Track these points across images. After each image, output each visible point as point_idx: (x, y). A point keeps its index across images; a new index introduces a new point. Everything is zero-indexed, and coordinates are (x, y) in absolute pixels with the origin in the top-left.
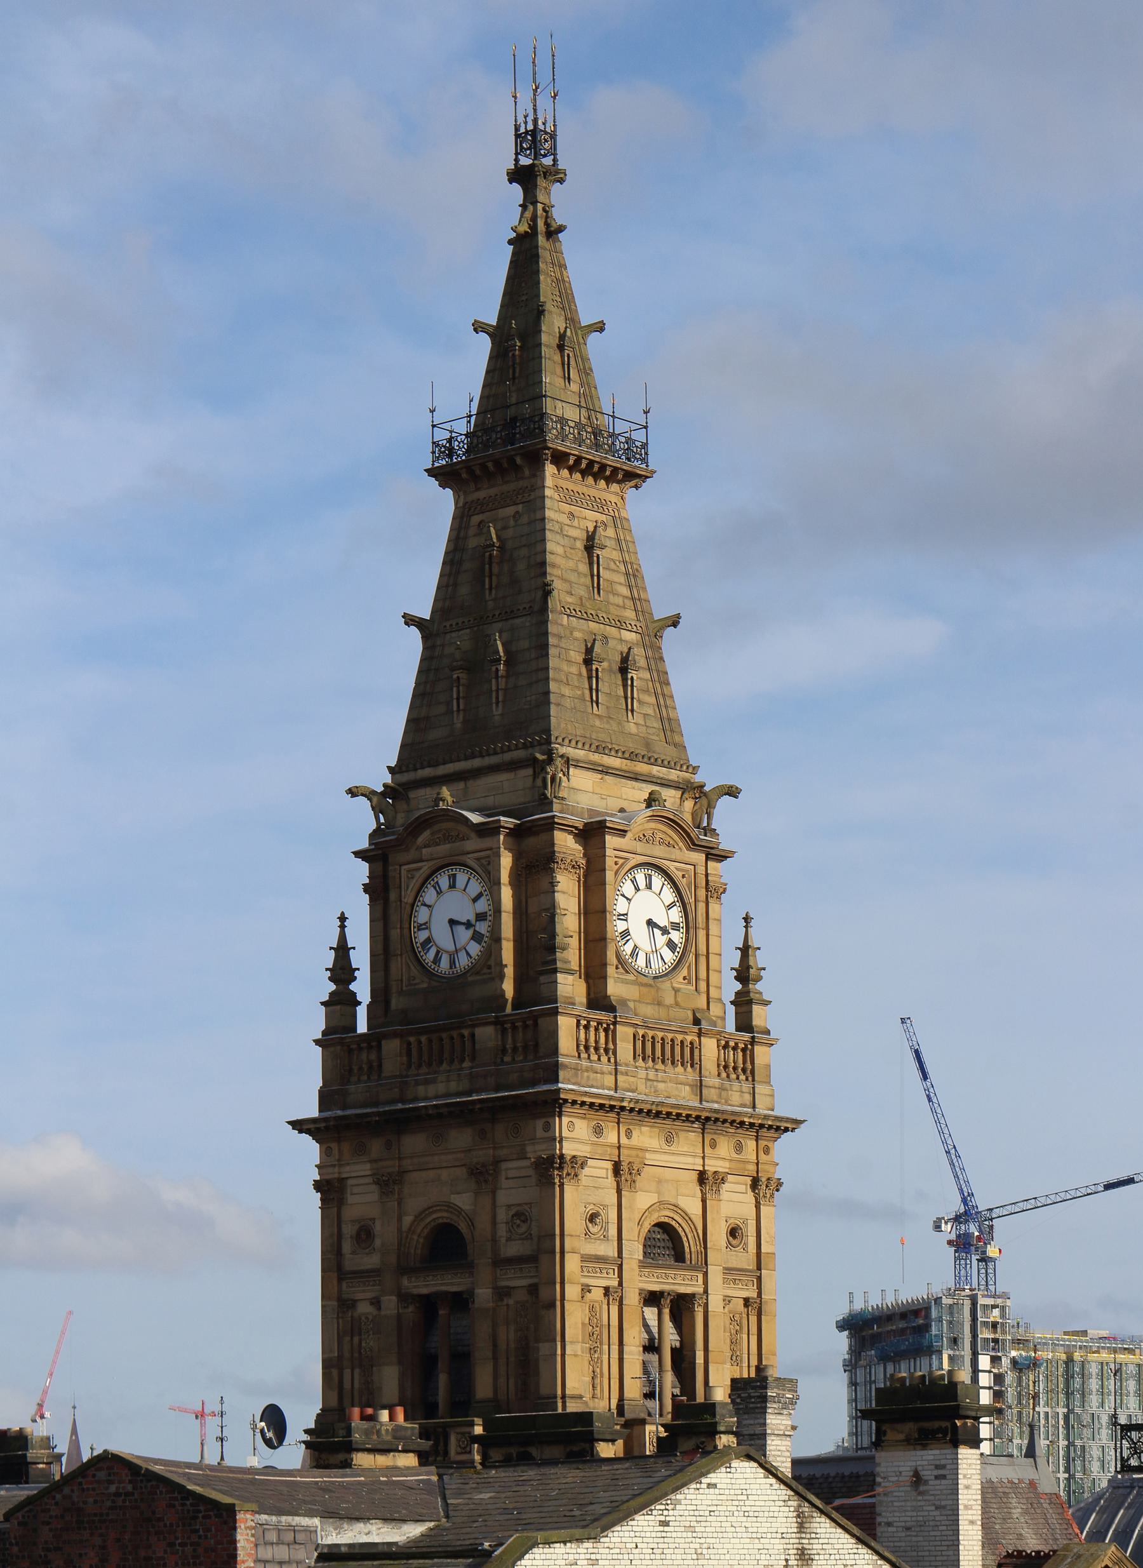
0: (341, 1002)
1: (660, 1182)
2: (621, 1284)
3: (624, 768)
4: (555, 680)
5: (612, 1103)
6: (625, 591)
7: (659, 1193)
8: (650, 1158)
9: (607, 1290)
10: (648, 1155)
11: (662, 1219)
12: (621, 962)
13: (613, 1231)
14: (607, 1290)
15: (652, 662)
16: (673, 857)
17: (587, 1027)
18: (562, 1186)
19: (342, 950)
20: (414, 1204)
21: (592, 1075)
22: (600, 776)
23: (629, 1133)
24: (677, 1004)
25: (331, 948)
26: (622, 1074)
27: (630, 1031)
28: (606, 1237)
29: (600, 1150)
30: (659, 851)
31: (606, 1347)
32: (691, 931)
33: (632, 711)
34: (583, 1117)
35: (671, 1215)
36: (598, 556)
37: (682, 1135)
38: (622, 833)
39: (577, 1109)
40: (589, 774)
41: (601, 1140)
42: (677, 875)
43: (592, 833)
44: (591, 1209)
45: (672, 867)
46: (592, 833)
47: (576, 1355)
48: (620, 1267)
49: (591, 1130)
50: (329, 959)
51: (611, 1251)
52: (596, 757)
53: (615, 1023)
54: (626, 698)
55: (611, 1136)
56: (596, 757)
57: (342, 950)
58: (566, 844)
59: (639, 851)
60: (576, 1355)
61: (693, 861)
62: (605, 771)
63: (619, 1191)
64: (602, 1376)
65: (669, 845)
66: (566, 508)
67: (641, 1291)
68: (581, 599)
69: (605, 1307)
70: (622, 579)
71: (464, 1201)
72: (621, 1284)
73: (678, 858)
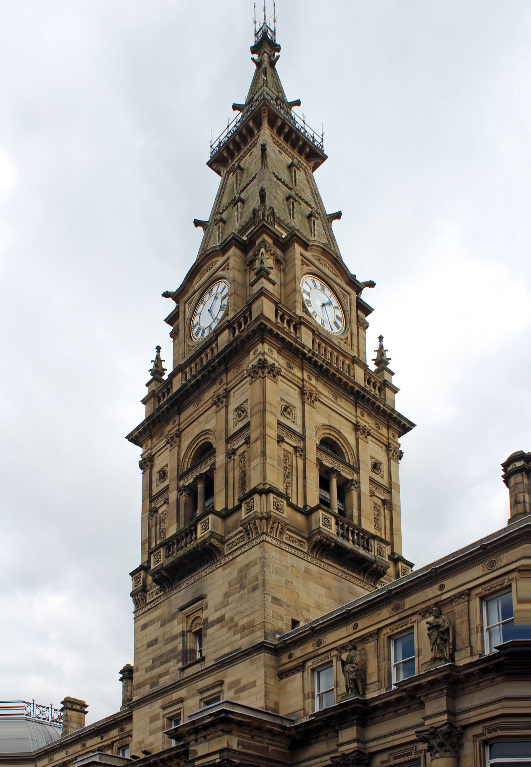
0: (157, 370)
7: (329, 420)
19: (158, 361)
20: (186, 441)
32: (348, 324)
50: (151, 366)
57: (158, 361)
71: (351, 438)
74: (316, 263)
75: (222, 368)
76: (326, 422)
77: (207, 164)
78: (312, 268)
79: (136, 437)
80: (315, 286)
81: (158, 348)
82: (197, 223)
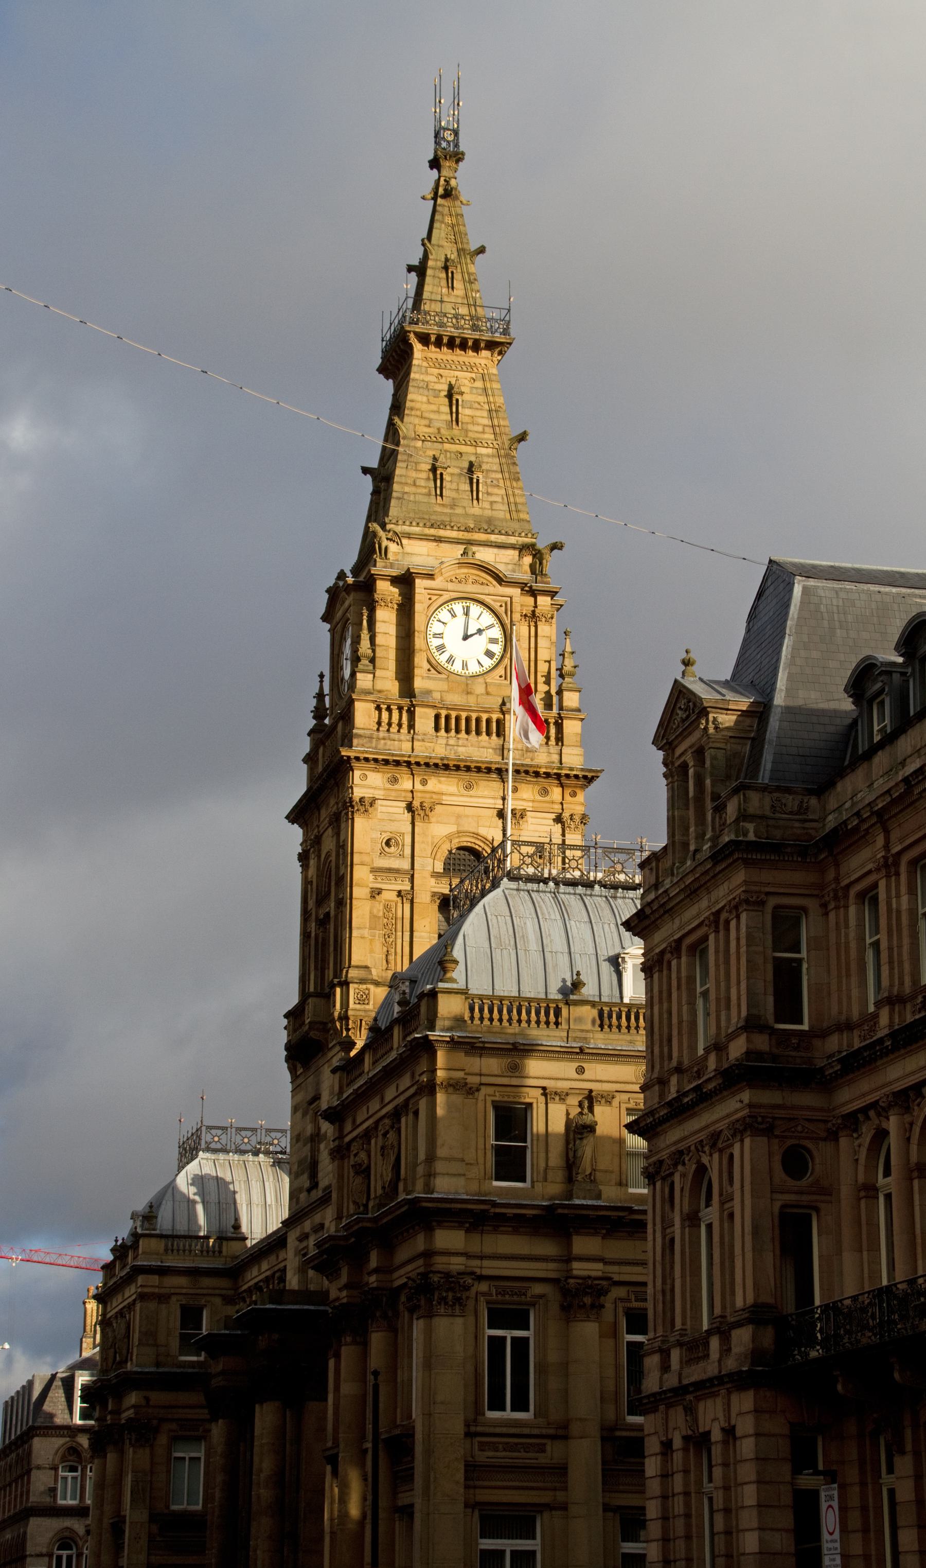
1: (459, 817)
2: (412, 888)
3: (460, 537)
4: (398, 483)
5: (367, 756)
6: (487, 422)
7: (458, 825)
8: (446, 799)
9: (399, 893)
10: (444, 797)
11: (465, 844)
12: (434, 666)
13: (408, 851)
14: (399, 893)
15: (505, 466)
16: (487, 592)
17: (389, 709)
18: (353, 819)
21: (389, 742)
22: (435, 544)
23: (424, 782)
24: (488, 693)
25: (365, 470)
26: (418, 740)
27: (432, 713)
28: (402, 856)
29: (393, 794)
30: (470, 588)
31: (399, 934)
33: (478, 499)
34: (375, 770)
35: (473, 840)
36: (457, 400)
37: (483, 784)
38: (431, 576)
39: (363, 764)
40: (424, 543)
41: (396, 787)
42: (496, 606)
43: (405, 581)
44: (386, 836)
45: (488, 600)
46: (405, 581)
47: (362, 938)
48: (413, 876)
49: (385, 780)
51: (406, 865)
52: (432, 531)
53: (414, 706)
54: (472, 491)
55: (406, 783)
56: (432, 531)
58: (384, 588)
59: (449, 588)
60: (362, 938)
61: (511, 594)
62: (439, 540)
63: (413, 824)
64: (396, 954)
65: (482, 584)
66: (436, 371)
67: (434, 894)
68: (439, 429)
69: (400, 905)
70: (485, 414)
72: (412, 888)
73: (492, 592)
74: (450, 586)
75: (333, 782)
76: (453, 829)
78: (447, 596)
79: (298, 815)
80: (454, 616)
81: (322, 676)
82: (365, 470)
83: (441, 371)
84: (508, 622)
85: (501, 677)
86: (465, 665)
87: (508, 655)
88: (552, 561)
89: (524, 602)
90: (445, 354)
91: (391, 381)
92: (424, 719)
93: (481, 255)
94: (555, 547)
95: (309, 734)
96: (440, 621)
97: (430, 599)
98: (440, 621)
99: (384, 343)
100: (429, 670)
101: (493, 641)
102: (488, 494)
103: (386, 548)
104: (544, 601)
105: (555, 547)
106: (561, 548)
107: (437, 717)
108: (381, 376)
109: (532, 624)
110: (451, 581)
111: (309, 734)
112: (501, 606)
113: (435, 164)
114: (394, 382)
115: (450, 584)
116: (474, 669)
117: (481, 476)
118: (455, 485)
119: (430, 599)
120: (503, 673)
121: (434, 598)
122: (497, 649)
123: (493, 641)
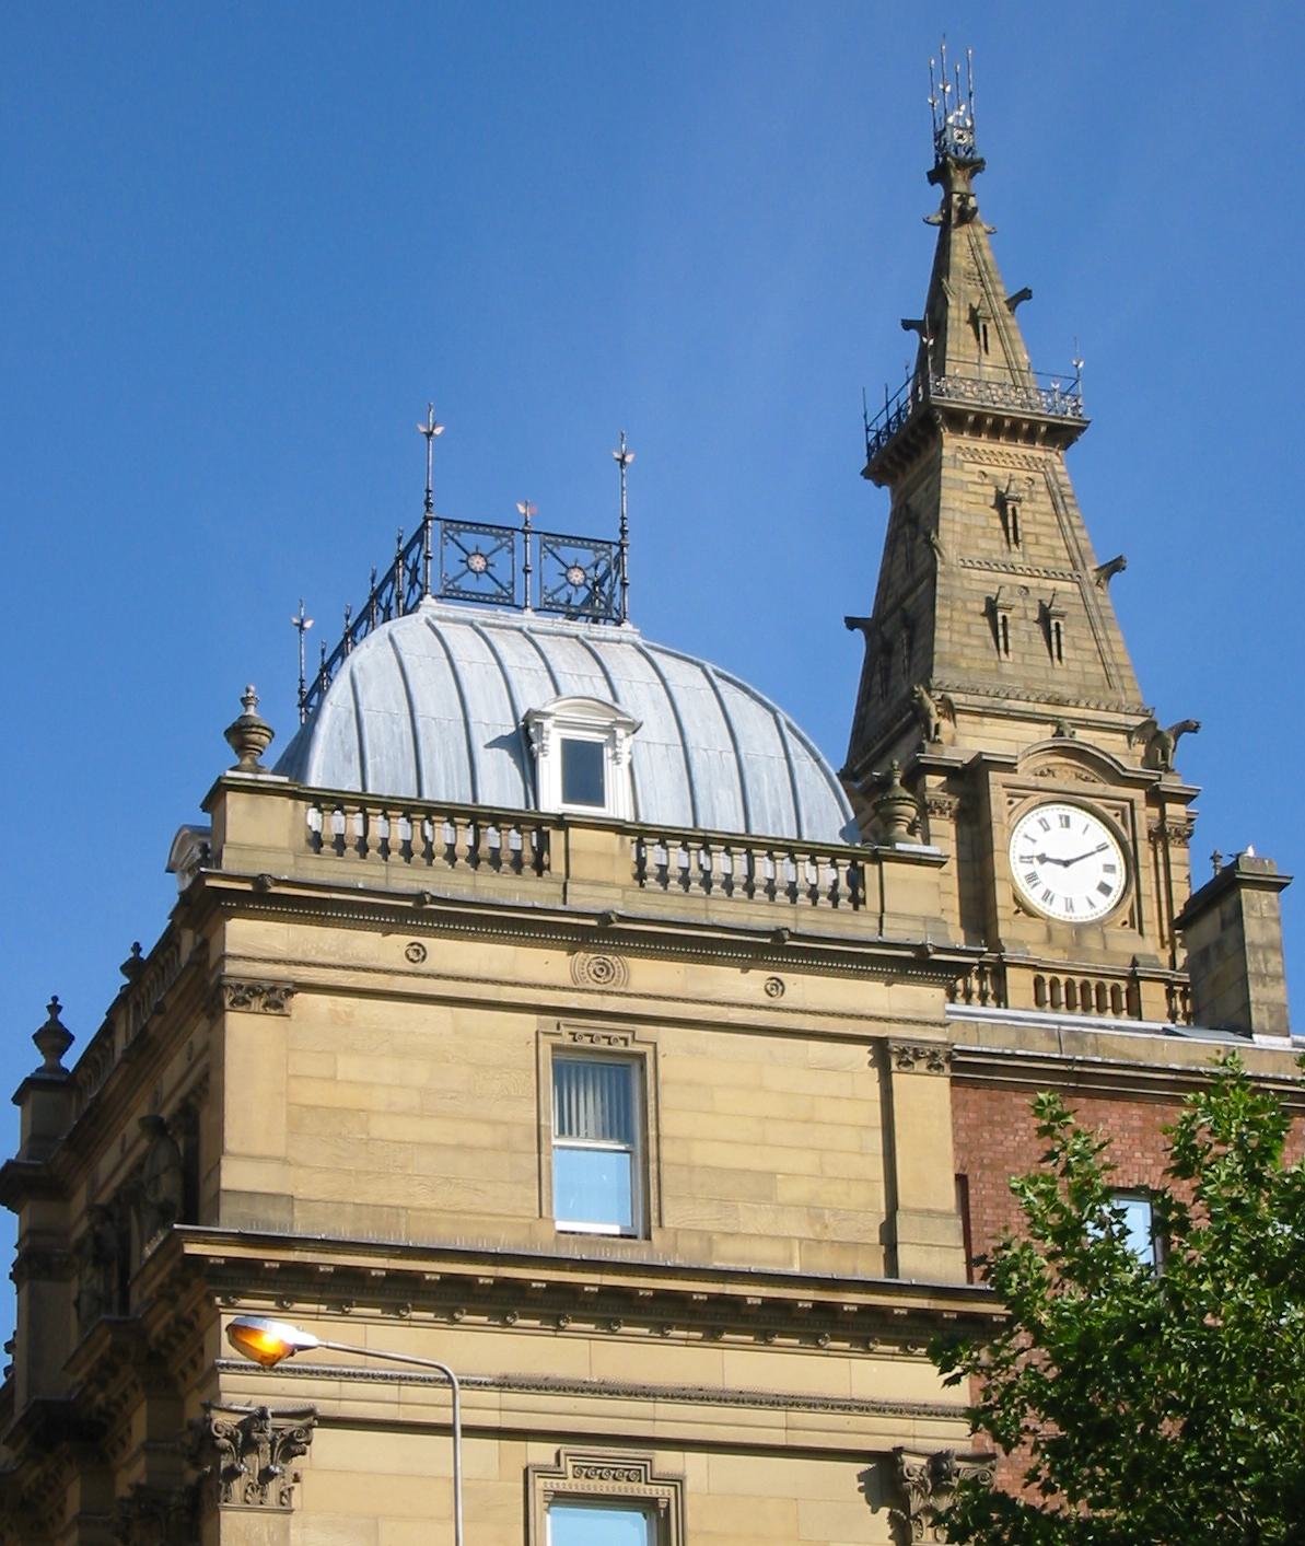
12: (1023, 907)
25: (852, 623)
27: (1030, 975)
38: (1009, 767)
45: (1097, 803)
61: (1130, 796)
77: (862, 473)
82: (852, 623)
83: (984, 468)
84: (1127, 836)
85: (1125, 923)
86: (1070, 907)
87: (1134, 891)
88: (1183, 752)
89: (1146, 816)
90: (983, 444)
91: (886, 490)
92: (1019, 982)
93: (1025, 302)
94: (1188, 727)
95: (18, 1099)
96: (1026, 836)
97: (1011, 803)
98: (1026, 836)
99: (872, 435)
100: (1018, 912)
101: (1110, 868)
102: (1076, 648)
103: (937, 726)
104: (1174, 810)
105: (1188, 727)
106: (1195, 729)
107: (1038, 982)
108: (870, 483)
109: (1160, 845)
110: (1042, 774)
111: (18, 1099)
112: (1117, 815)
113: (940, 175)
114: (893, 492)
115: (1040, 778)
116: (1083, 914)
117: (1061, 623)
118: (1024, 631)
119: (1011, 803)
120: (1127, 918)
121: (1017, 801)
122: (1117, 881)
123: (1110, 868)
